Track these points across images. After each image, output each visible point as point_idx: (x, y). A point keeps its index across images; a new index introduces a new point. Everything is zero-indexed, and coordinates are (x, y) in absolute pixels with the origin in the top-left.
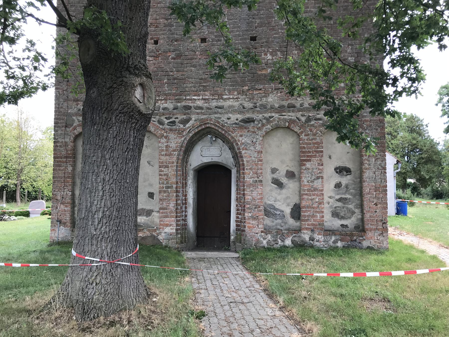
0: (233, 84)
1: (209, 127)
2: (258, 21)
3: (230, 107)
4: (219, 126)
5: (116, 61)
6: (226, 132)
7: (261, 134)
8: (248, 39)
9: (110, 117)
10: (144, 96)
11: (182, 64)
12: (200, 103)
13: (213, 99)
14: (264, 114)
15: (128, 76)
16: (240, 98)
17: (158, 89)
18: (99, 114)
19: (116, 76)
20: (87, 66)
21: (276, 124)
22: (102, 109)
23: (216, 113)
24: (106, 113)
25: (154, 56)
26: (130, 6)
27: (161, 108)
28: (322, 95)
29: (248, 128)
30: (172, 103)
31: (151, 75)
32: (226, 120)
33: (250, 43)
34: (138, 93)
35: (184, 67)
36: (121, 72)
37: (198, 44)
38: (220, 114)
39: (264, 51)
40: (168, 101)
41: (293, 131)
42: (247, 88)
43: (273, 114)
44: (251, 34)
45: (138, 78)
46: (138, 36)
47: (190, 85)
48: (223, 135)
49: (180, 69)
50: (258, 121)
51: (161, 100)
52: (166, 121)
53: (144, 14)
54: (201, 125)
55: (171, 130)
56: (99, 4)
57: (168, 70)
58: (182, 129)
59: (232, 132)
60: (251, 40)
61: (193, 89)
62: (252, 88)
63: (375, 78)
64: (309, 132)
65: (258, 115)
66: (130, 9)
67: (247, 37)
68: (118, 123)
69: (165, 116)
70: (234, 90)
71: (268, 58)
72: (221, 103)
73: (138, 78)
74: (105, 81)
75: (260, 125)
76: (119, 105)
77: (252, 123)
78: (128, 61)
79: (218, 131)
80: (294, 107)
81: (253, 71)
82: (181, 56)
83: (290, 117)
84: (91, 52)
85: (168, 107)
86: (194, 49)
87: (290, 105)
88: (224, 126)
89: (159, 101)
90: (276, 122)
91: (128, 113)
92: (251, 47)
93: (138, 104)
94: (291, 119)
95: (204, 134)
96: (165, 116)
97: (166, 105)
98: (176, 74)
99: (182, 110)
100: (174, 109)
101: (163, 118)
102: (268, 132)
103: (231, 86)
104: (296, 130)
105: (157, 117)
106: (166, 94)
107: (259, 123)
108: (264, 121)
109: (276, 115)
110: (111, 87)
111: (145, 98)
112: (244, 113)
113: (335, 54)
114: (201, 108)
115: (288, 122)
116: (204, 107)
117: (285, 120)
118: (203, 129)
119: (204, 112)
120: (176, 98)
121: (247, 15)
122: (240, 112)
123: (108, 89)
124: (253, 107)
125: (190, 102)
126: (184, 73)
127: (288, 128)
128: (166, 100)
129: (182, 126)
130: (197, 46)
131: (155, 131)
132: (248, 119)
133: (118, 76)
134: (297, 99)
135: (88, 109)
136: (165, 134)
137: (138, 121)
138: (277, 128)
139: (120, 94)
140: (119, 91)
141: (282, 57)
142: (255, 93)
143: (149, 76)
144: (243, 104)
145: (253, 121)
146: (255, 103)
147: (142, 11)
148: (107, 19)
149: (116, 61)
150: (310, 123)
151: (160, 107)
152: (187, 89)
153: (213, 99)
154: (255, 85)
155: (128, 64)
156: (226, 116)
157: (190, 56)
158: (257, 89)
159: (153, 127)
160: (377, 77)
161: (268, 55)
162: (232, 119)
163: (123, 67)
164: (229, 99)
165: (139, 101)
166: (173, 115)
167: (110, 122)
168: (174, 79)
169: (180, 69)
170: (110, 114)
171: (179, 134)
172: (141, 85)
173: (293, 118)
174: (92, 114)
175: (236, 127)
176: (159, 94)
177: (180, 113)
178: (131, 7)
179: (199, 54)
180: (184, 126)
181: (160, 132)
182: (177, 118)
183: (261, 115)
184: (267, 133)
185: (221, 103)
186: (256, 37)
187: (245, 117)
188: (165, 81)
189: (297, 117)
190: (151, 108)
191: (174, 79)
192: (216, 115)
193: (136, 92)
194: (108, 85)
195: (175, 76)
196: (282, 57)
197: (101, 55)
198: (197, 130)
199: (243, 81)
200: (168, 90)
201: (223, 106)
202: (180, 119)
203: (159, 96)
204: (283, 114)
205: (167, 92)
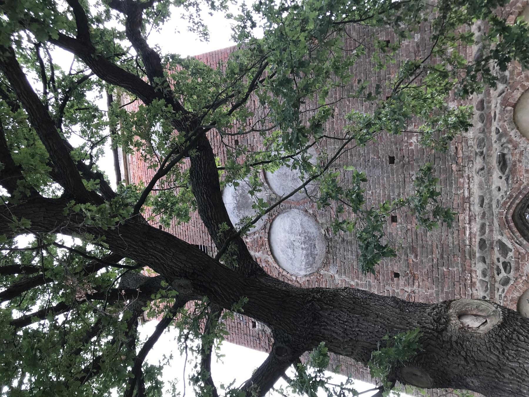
0: (449, 184)
1: (513, 217)
2: (371, 156)
3: (481, 187)
4: (511, 203)
5: (429, 344)
6: (520, 193)
7: (524, 143)
8: (392, 166)
9: (509, 369)
10: (475, 315)
11: (423, 247)
12: (476, 228)
13: (470, 210)
14: (493, 142)
15: (449, 334)
16: (469, 175)
17: (456, 280)
18: (504, 383)
19: (450, 350)
20: (436, 383)
21: (509, 124)
22: (497, 378)
23: (490, 207)
24: (504, 374)
25: (414, 280)
26: (363, 315)
27: (484, 279)
28: (473, 77)
29: (515, 161)
30: (475, 264)
31: (445, 301)
32: (502, 193)
33: (397, 163)
34: (471, 323)
35: (428, 244)
36: (443, 341)
37: (398, 226)
38: (491, 201)
39: (407, 146)
40: (473, 268)
41: (519, 99)
42: (454, 166)
43: (493, 129)
44: (386, 164)
45: (450, 320)
46: (398, 311)
47: (450, 238)
48: (525, 196)
49: (429, 250)
50: (503, 149)
51: (471, 277)
52: (503, 274)
53: (371, 299)
54: (510, 228)
55: (517, 269)
56: (362, 350)
57: (430, 264)
58: (515, 254)
59: (521, 185)
60: (394, 163)
61: (455, 235)
62: (454, 159)
63: (451, 9)
64: (523, 76)
65: (494, 150)
66: (367, 315)
67: (390, 168)
68: (519, 359)
69: (496, 275)
70: (457, 182)
71: (415, 141)
72: (475, 199)
73: (450, 320)
74: (456, 365)
75: (510, 146)
76: (492, 353)
77: (507, 157)
78: (429, 329)
79: (518, 204)
80: (482, 102)
81: (432, 158)
82: (413, 246)
83: (498, 105)
84: (419, 374)
85: (481, 269)
86: (404, 231)
87: (479, 107)
88: (511, 196)
89: (473, 280)
90: (505, 123)
91: (503, 343)
92: (401, 163)
93: (489, 325)
94: (502, 104)
95: (524, 224)
96: (496, 275)
97: (479, 273)
98: (436, 255)
99: (486, 252)
100: (485, 262)
101: (498, 278)
102: (521, 133)
103: (451, 186)
104: (519, 95)
105: (497, 285)
106: (464, 271)
107: (507, 147)
108: (504, 140)
109: (495, 125)
110: (465, 359)
111: (479, 314)
112: (490, 169)
113: (418, 67)
114: (483, 226)
115: (506, 107)
116: (481, 222)
117: (503, 111)
118: (516, 225)
119: (489, 223)
120: (468, 258)
121: (365, 169)
122: (490, 173)
123: (468, 363)
124: (482, 157)
125: (473, 240)
126: (435, 246)
127: (515, 106)
128: (471, 272)
129: (510, 254)
130: (401, 228)
131: (519, 291)
132: (499, 163)
133: (449, 347)
134: (471, 100)
135: (497, 394)
136: (524, 278)
137: (515, 330)
138: (515, 122)
139: (476, 350)
140: (471, 349)
141: (413, 124)
142: (461, 155)
143: (448, 304)
144: (477, 170)
145: (503, 155)
146: (476, 154)
147: (368, 302)
148: (380, 352)
149: (429, 344)
150: (508, 77)
151: (481, 280)
152: (456, 243)
153: (470, 210)
154: (451, 156)
155: (433, 330)
156: (495, 192)
157: (413, 236)
158: (456, 153)
159: (513, 293)
160: (452, 6)
161: (411, 141)
162: (500, 184)
163: (437, 338)
164: (469, 188)
165: (483, 324)
166: (493, 263)
167: (517, 370)
168: (442, 257)
169: (429, 250)
170: (505, 368)
171: (524, 258)
172: (461, 316)
173: (499, 101)
174: (504, 391)
175: (513, 178)
176: (463, 279)
177: (491, 255)
178: (364, 314)
179: (410, 225)
180: (511, 251)
181: (520, 285)
182: (498, 260)
183: (495, 145)
184: (523, 135)
185: (475, 199)
186: (390, 157)
187: (496, 167)
188: (445, 270)
189: (499, 96)
190: (494, 309)
191: (442, 257)
192: (494, 206)
193: (471, 326)
194: (463, 362)
195: (438, 256)
196: (413, 124)
197: (422, 362)
198: (518, 234)
199: (445, 171)
200: (457, 266)
201: (480, 196)
202: (499, 256)
203: (466, 280)
204: (493, 115)
205: (460, 269)
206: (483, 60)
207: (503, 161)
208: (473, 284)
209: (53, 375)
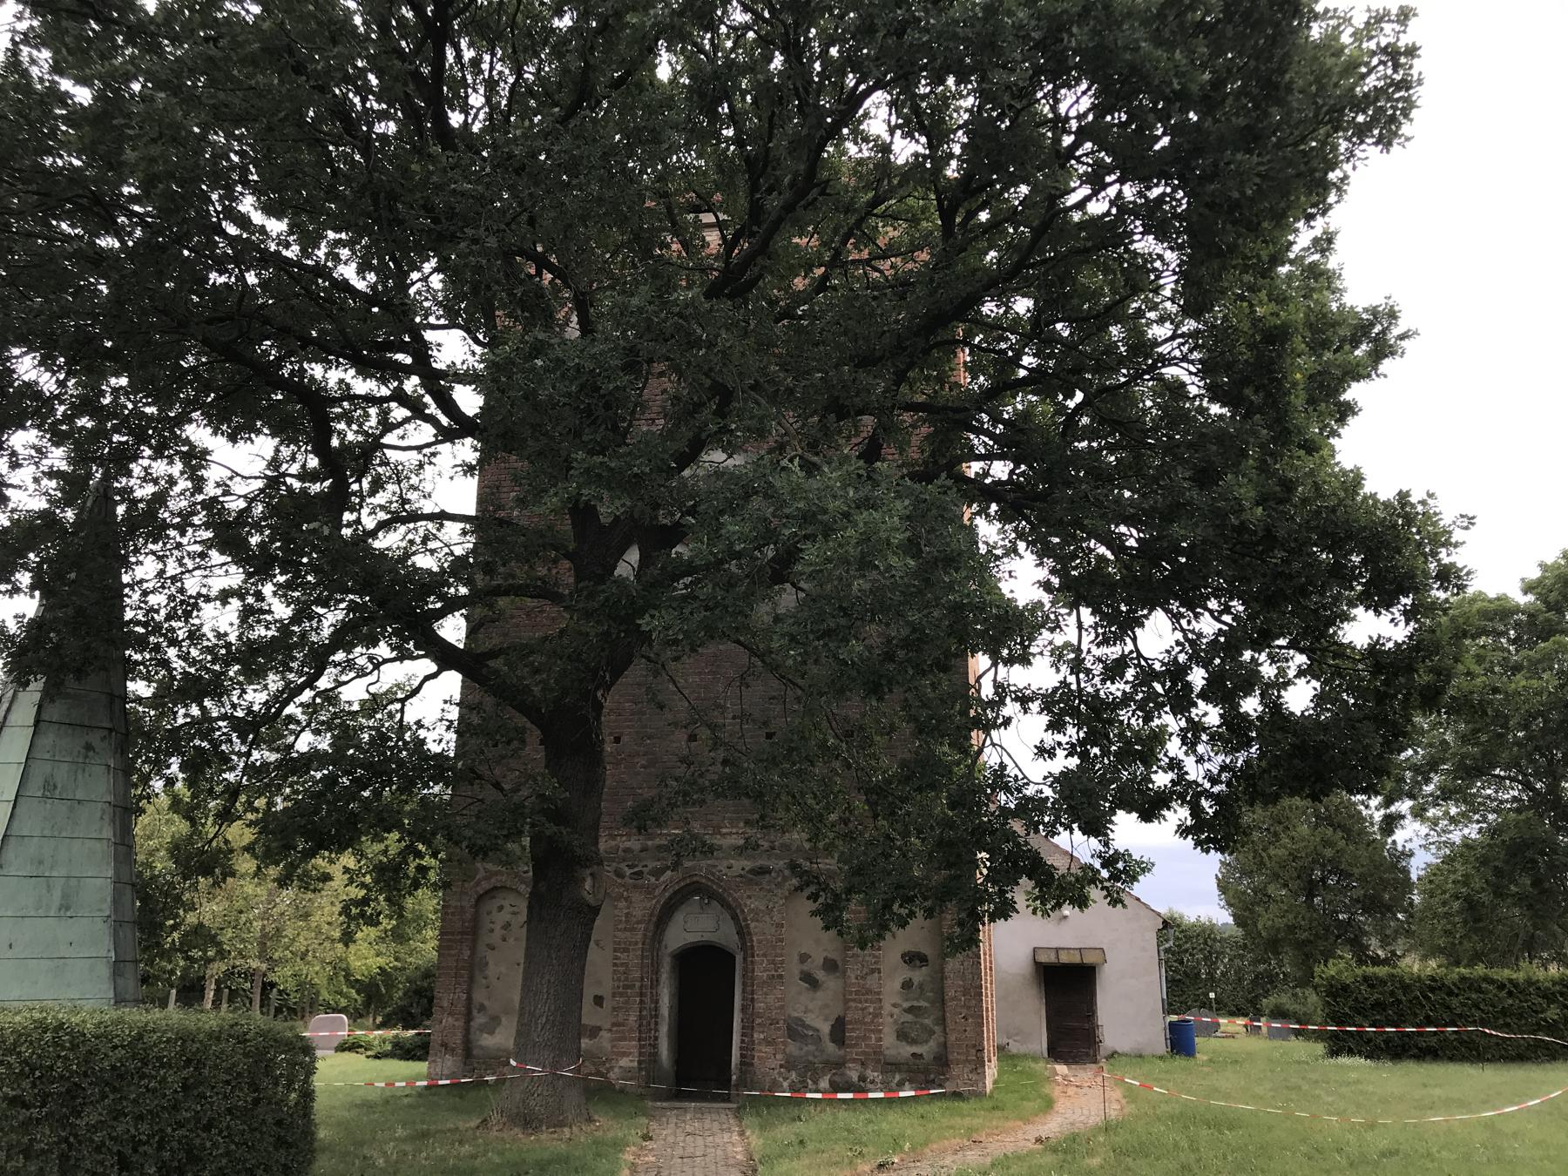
52: (628, 872)
55: (635, 886)
97: (628, 844)
101: (623, 866)
129: (653, 879)
145: (769, 872)
156: (725, 863)
206: (442, 597)
207: (763, 871)
208: (613, 837)
209: (980, 387)
